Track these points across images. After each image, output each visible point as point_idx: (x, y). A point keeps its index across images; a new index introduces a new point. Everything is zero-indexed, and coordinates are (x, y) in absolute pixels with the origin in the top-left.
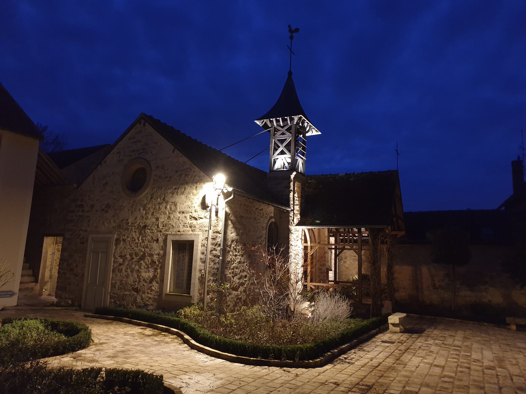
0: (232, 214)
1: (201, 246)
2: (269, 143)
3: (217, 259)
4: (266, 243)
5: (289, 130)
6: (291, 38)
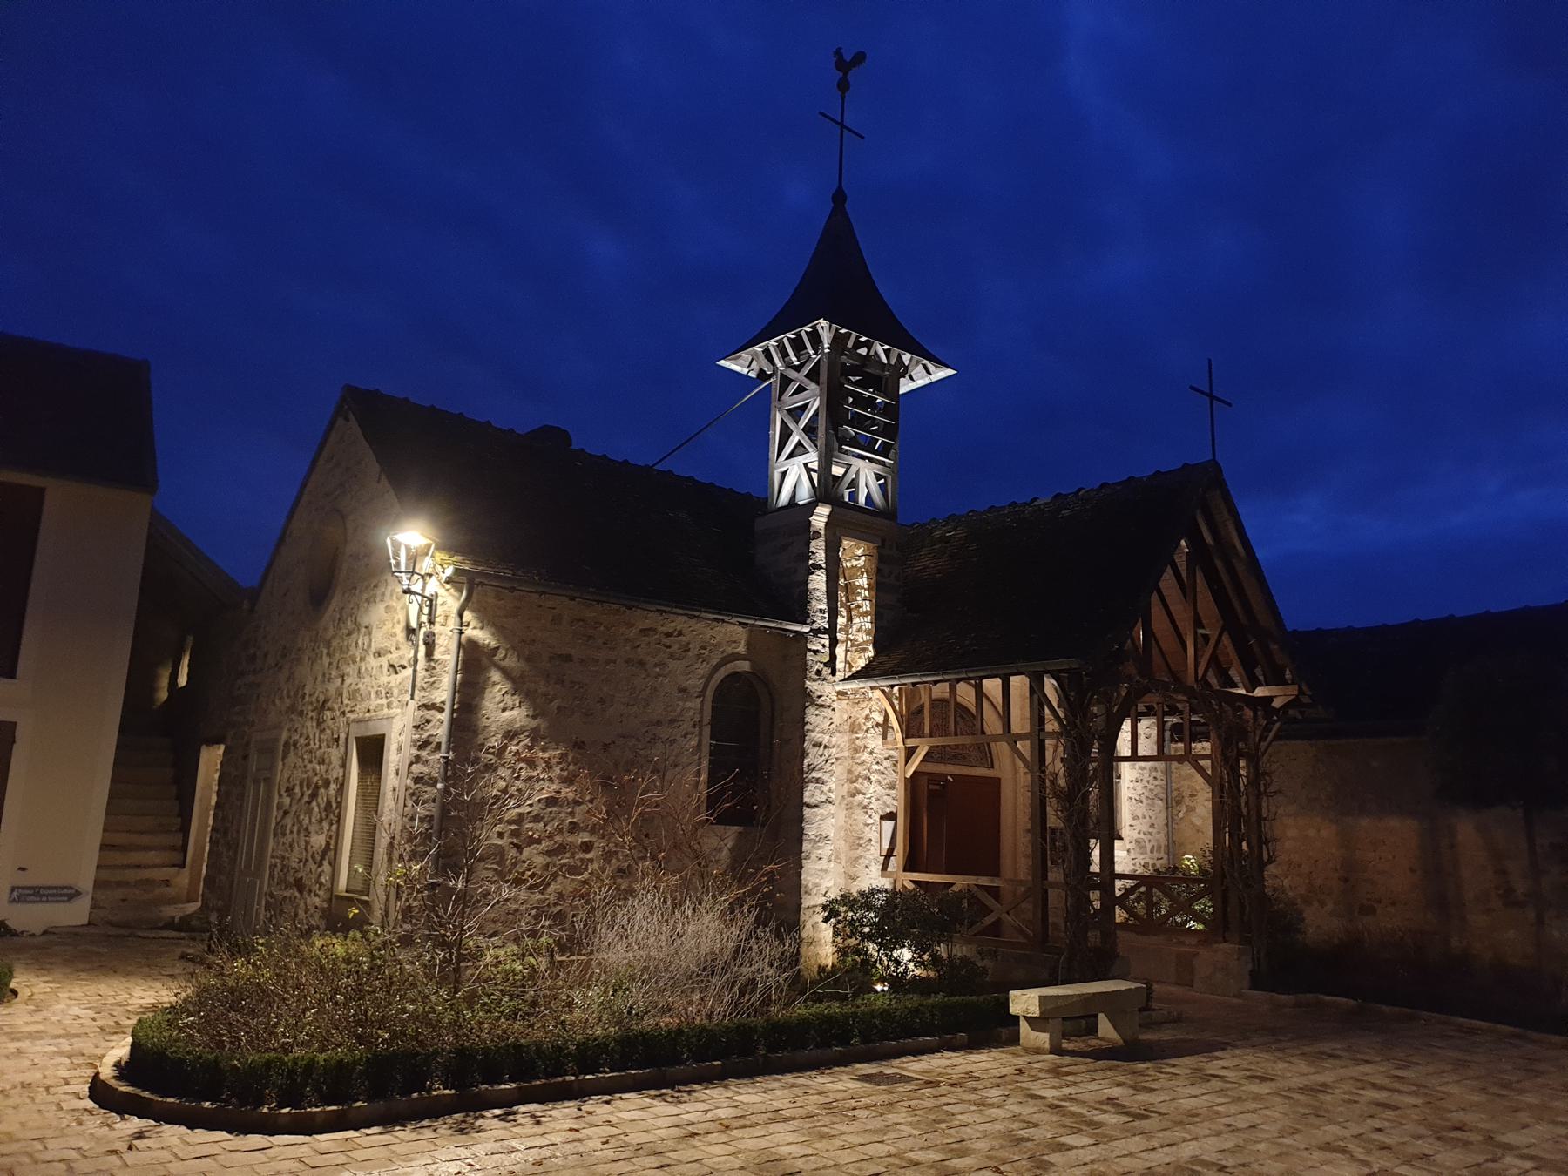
0: (507, 650)
1: (396, 752)
2: (767, 424)
3: (428, 789)
4: (700, 741)
5: (813, 375)
6: (843, 86)
